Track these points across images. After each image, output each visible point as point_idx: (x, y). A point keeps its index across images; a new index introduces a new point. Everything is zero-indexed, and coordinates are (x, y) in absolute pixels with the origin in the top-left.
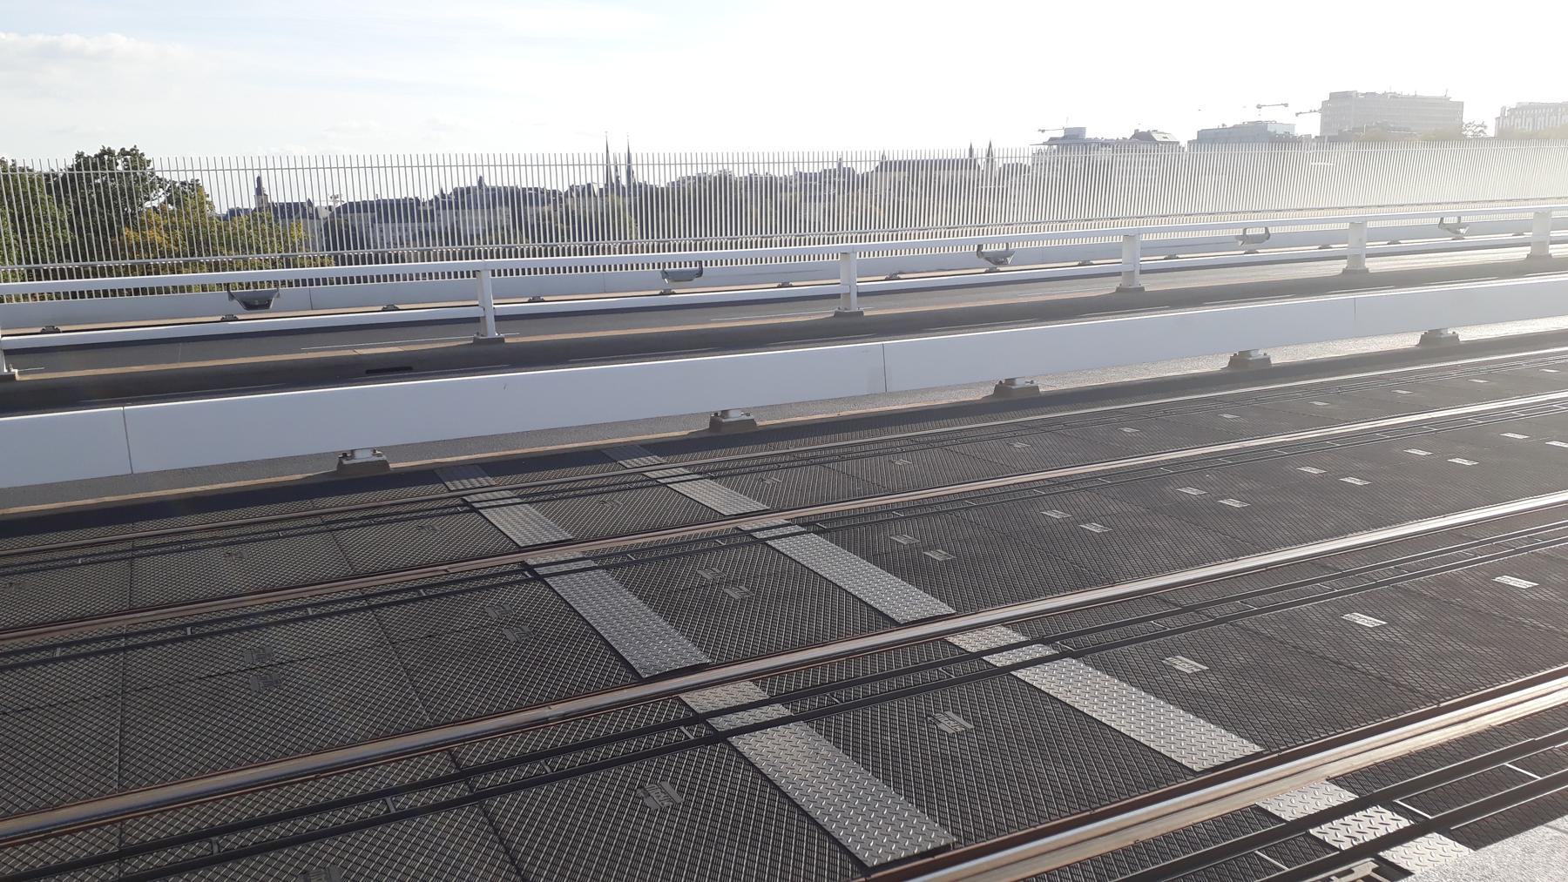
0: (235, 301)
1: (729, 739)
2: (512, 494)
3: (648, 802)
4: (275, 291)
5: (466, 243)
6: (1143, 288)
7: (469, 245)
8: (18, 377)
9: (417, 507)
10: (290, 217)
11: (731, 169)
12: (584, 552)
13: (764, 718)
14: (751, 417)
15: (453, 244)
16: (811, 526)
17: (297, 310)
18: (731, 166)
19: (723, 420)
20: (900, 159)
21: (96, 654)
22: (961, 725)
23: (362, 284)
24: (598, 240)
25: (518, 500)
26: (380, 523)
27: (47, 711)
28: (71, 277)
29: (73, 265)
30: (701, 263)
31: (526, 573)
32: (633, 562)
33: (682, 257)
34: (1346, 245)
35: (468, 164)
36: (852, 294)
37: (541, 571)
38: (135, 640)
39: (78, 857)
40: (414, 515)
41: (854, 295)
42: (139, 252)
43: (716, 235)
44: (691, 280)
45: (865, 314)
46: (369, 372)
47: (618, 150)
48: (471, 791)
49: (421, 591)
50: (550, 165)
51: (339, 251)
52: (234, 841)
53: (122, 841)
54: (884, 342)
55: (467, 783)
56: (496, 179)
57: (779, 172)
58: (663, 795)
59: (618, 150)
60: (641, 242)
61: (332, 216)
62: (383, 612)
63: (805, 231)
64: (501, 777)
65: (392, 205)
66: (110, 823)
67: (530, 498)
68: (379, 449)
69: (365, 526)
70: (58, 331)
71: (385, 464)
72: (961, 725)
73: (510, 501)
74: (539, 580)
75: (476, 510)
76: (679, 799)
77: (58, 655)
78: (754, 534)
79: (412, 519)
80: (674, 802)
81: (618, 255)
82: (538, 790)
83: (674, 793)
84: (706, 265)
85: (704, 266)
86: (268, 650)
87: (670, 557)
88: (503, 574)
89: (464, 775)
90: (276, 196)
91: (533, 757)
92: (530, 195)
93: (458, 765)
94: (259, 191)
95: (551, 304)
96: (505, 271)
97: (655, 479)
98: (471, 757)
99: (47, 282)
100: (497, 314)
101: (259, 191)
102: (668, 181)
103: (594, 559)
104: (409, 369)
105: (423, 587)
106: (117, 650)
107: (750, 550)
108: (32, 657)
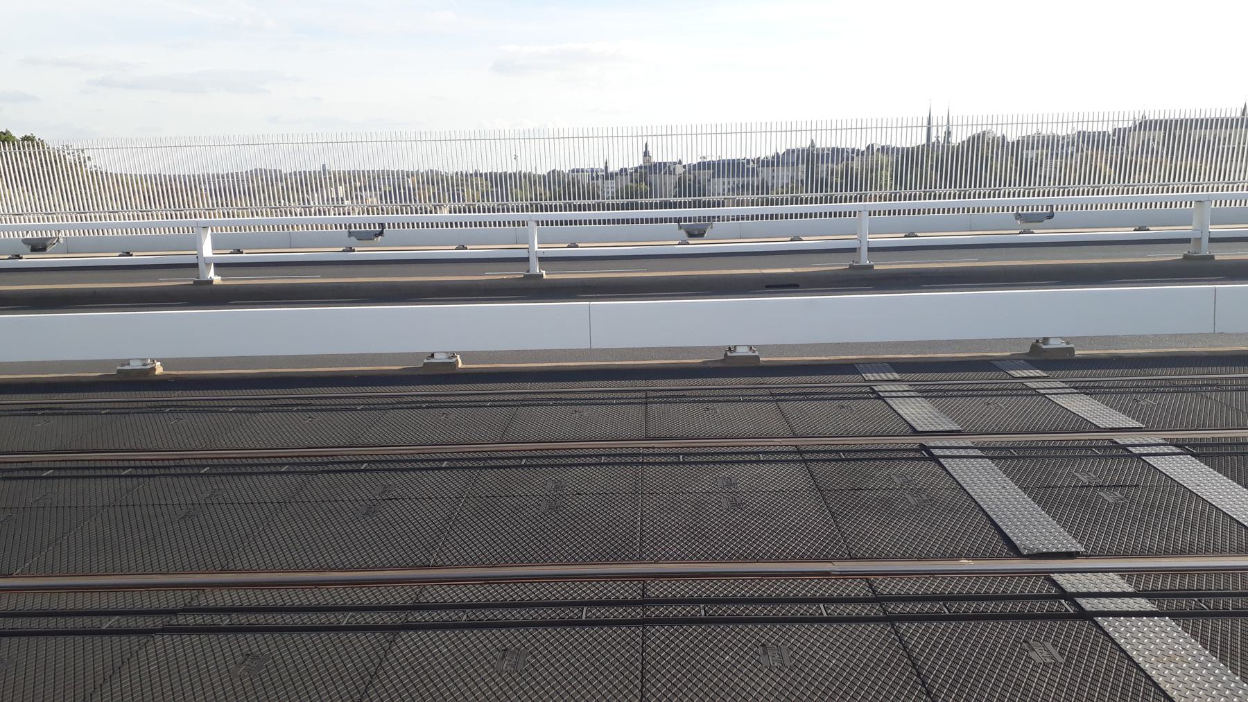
0: (682, 230)
1: (1095, 619)
2: (911, 388)
3: (1032, 655)
4: (709, 225)
5: (502, 200)
6: (1212, 257)
7: (505, 202)
8: (545, 277)
9: (583, 396)
10: (655, 173)
11: (994, 130)
12: (973, 443)
13: (1125, 608)
14: (1071, 346)
15: (459, 201)
16: (1186, 448)
17: (1235, 224)
18: (995, 127)
19: (1044, 347)
20: (1192, 117)
21: (626, 464)
22: (1053, 658)
23: (569, 226)
24: (970, 187)
25: (913, 394)
26: (811, 400)
27: (578, 497)
28: (623, 209)
29: (750, 197)
30: (1052, 207)
31: (923, 452)
32: (1016, 457)
33: (1034, 202)
34: (855, 237)
35: (785, 129)
36: (862, 248)
37: (937, 452)
38: (544, 461)
39: (575, 599)
40: (713, 398)
41: (864, 252)
42: (743, 191)
43: (1084, 184)
44: (1042, 221)
45: (1216, 258)
46: (768, 287)
47: (939, 116)
48: (885, 613)
49: (841, 454)
50: (826, 130)
51: (539, 201)
52: (488, 614)
53: (644, 593)
54: (1217, 286)
55: (881, 606)
56: (1046, 131)
57: (1063, 131)
58: (778, 656)
59: (939, 116)
60: (983, 190)
61: (685, 173)
62: (812, 465)
63: (1169, 181)
64: (908, 608)
65: (729, 164)
66: (497, 583)
67: (926, 393)
68: (755, 346)
69: (800, 400)
70: (688, 244)
71: (1072, 350)
72: (1053, 658)
73: (906, 394)
74: (934, 459)
75: (880, 398)
76: (1060, 659)
77: (602, 461)
78: (933, 450)
79: (835, 399)
80: (1056, 660)
81: (467, 214)
82: (929, 625)
83: (1055, 653)
84: (1057, 209)
85: (1054, 210)
86: (733, 481)
87: (1082, 457)
88: (620, 455)
89: (880, 599)
90: (656, 158)
91: (934, 598)
92: (828, 154)
93: (874, 591)
94: (646, 154)
95: (923, 238)
96: (427, 224)
97: (1034, 389)
98: (884, 587)
99: (609, 212)
100: (1211, 237)
101: (646, 154)
102: (1019, 134)
103: (981, 449)
104: (796, 286)
105: (843, 451)
106: (638, 464)
107: (1106, 463)
108: (718, 458)
